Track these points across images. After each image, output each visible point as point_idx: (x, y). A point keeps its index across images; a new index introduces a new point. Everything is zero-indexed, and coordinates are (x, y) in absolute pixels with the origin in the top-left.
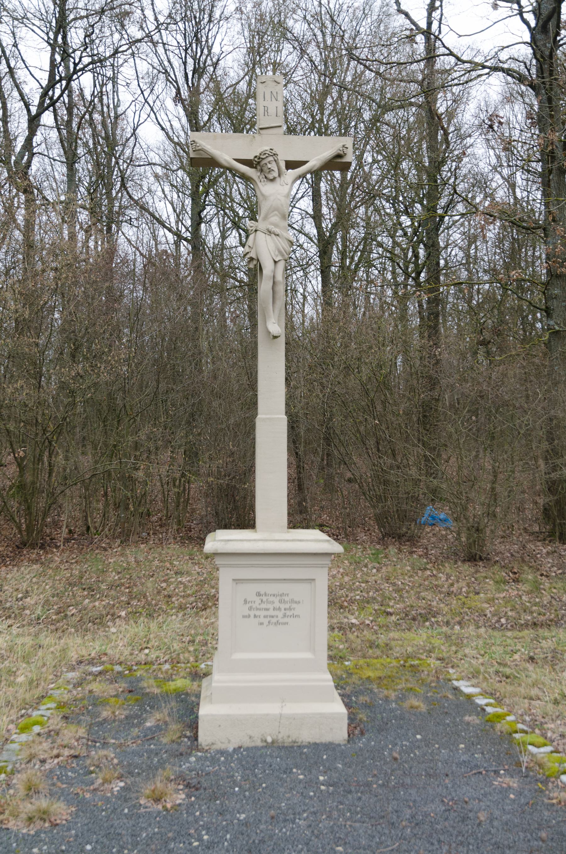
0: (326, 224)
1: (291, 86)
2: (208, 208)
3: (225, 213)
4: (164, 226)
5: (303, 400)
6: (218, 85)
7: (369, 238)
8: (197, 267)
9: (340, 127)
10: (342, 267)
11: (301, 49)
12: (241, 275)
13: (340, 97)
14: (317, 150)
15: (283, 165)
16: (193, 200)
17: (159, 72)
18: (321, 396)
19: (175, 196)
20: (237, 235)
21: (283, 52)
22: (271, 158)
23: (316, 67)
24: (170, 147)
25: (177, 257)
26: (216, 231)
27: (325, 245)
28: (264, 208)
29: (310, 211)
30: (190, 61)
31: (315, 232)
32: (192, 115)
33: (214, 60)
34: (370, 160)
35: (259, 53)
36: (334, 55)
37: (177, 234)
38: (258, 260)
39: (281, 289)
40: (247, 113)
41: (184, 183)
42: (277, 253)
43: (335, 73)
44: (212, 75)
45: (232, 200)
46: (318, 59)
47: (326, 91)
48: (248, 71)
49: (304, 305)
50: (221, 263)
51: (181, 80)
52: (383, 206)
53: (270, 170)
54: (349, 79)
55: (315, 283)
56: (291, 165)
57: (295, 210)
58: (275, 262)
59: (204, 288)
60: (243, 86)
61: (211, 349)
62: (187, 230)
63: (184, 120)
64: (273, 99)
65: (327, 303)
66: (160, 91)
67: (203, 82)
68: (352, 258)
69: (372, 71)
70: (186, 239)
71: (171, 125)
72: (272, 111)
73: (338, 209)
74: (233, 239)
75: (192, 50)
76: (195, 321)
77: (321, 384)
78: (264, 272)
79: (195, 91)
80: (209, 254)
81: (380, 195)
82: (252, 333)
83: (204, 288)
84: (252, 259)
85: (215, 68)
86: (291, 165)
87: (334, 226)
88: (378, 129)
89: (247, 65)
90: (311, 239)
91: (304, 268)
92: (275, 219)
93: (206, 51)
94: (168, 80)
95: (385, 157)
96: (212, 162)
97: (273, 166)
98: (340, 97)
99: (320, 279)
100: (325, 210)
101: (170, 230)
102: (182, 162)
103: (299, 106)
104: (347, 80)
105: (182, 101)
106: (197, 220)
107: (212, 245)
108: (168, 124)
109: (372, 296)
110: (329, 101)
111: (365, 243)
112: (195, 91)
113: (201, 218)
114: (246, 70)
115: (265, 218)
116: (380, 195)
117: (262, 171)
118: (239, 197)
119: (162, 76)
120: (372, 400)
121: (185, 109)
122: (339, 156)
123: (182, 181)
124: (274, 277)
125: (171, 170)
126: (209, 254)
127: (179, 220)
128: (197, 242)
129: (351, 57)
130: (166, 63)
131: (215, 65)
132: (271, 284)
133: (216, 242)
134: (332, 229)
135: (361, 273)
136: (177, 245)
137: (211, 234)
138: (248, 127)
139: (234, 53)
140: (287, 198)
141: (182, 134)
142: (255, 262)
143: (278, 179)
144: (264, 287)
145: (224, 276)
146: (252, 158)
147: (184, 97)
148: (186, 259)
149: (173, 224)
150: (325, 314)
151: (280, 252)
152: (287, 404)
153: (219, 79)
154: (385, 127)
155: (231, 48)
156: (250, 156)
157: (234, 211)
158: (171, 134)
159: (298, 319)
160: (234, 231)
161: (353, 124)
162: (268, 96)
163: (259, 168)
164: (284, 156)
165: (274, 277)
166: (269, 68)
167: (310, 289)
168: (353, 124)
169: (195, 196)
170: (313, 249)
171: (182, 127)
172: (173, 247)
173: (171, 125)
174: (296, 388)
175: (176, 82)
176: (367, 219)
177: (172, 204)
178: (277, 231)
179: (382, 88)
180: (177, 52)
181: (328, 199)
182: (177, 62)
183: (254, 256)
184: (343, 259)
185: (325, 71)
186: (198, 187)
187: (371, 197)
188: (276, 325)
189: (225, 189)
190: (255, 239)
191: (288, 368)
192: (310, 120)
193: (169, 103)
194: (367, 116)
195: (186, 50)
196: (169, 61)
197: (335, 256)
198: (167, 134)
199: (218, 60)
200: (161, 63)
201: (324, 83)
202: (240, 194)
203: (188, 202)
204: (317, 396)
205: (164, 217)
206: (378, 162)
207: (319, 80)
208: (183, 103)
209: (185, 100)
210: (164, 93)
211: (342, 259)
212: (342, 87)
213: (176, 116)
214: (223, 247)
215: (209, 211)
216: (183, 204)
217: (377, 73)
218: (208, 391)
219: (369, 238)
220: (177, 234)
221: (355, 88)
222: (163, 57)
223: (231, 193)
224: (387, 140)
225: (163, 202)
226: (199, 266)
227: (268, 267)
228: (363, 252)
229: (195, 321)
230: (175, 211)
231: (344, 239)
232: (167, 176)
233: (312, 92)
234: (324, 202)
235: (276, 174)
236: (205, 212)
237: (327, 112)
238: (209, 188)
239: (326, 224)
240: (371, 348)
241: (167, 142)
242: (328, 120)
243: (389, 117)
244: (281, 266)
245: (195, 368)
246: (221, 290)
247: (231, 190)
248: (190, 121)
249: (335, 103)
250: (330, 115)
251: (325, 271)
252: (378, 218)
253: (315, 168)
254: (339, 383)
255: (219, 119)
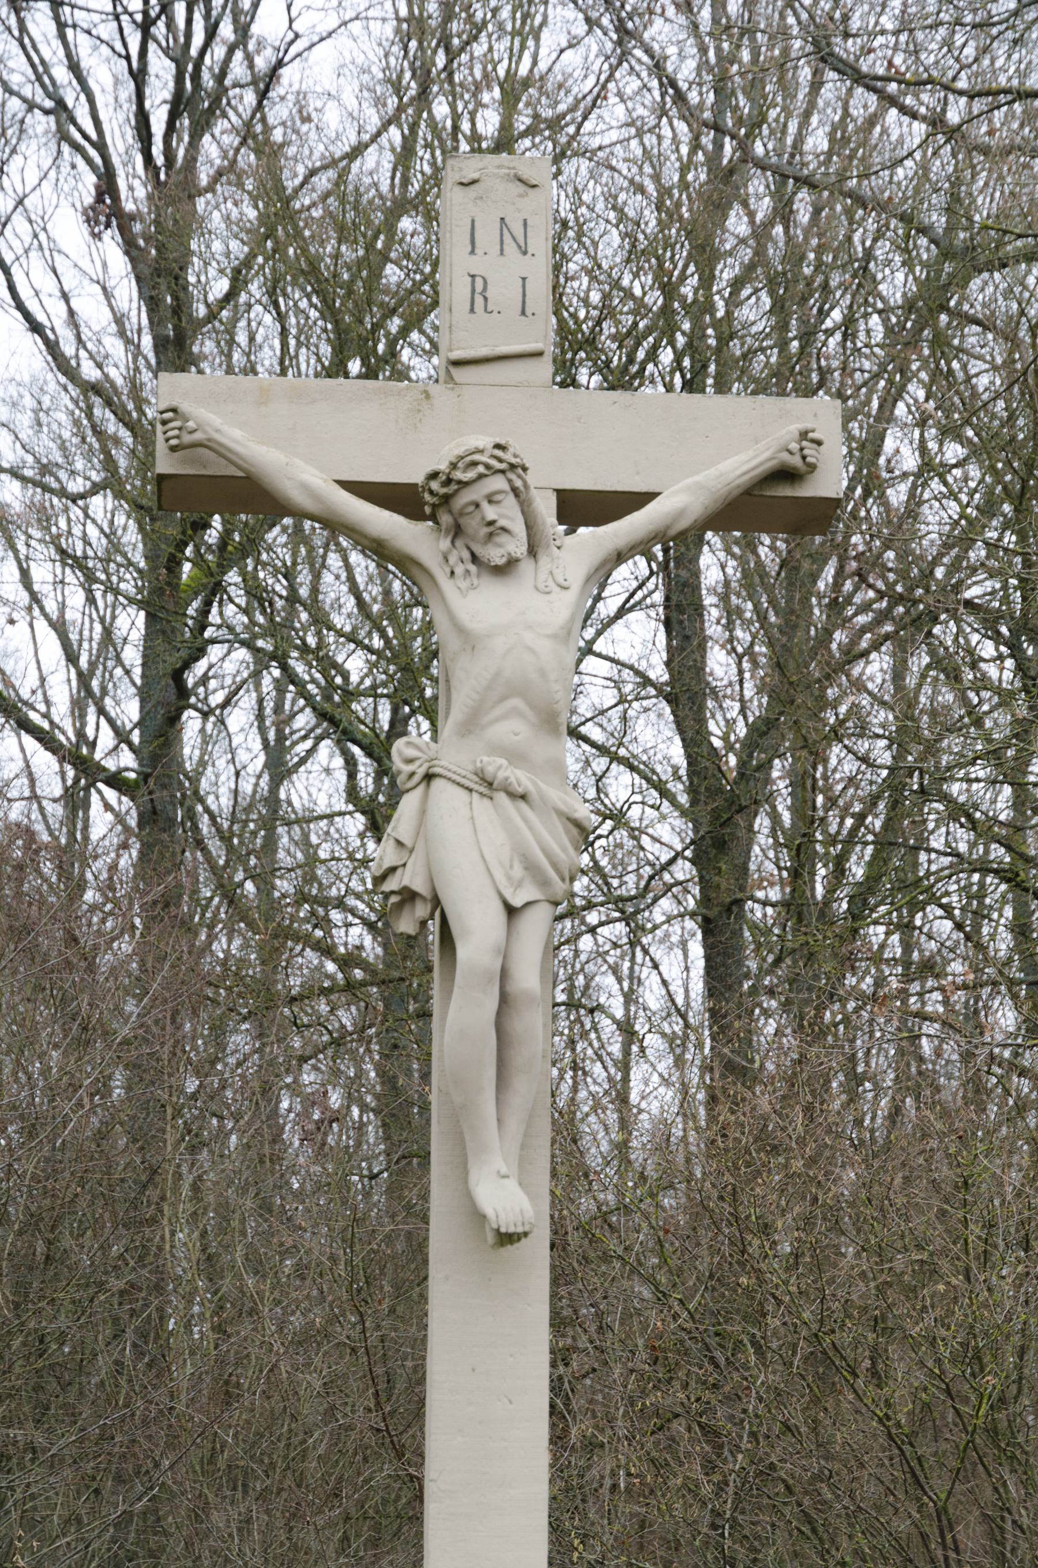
0: (726, 724)
1: (577, 168)
2: (215, 652)
3: (290, 676)
4: (25, 725)
5: (626, 1508)
6: (270, 153)
7: (910, 790)
8: (165, 908)
9: (783, 327)
10: (795, 906)
11: (621, 28)
12: (354, 936)
13: (784, 212)
14: (692, 448)
15: (546, 507)
16: (151, 618)
17: (31, 106)
18: (707, 1490)
19: (76, 598)
20: (338, 762)
21: (545, 35)
22: (498, 483)
23: (680, 97)
24: (63, 404)
25: (73, 854)
26: (253, 756)
27: (719, 808)
28: (465, 681)
29: (659, 673)
30: (161, 70)
31: (677, 752)
32: (161, 271)
33: (261, 63)
34: (910, 461)
35: (445, 42)
36: (755, 53)
37: (79, 759)
38: (436, 902)
39: (533, 1026)
40: (390, 269)
41: (115, 546)
42: (518, 871)
43: (758, 121)
44: (248, 125)
45: (321, 621)
46: (691, 64)
47: (725, 186)
48: (400, 109)
49: (625, 1067)
50: (264, 879)
51: (120, 139)
52: (970, 651)
53: (494, 530)
54: (818, 141)
55: (679, 965)
56: (580, 508)
57: (591, 664)
58: (511, 911)
59: (183, 990)
60: (377, 167)
61: (210, 1264)
62: (122, 736)
63: (127, 294)
64: (510, 247)
65: (733, 1067)
66: (32, 179)
67: (209, 148)
68: (839, 870)
69: (914, 116)
70: (115, 781)
71: (71, 313)
72: (503, 292)
73: (779, 666)
74: (319, 782)
75: (170, 25)
76: (143, 1139)
77: (710, 1433)
78: (462, 952)
79: (176, 187)
80: (215, 846)
81: (951, 602)
82: (393, 1190)
83: (183, 990)
84: (409, 896)
85: (262, 95)
86: (580, 508)
87: (762, 731)
88: (940, 342)
89: (398, 88)
90: (665, 793)
91: (630, 910)
92: (512, 728)
93: (226, 30)
94: (63, 136)
95: (975, 452)
96: (253, 498)
97: (507, 513)
98: (784, 212)
99: (697, 949)
100: (719, 664)
101: (46, 740)
102: (109, 464)
103: (611, 246)
104: (809, 144)
105: (123, 221)
106: (169, 696)
107: (226, 801)
108: (58, 310)
109: (931, 1028)
110: (737, 223)
111: (894, 805)
112: (176, 187)
113: (183, 692)
114: (392, 102)
115: (470, 726)
116: (951, 602)
117: (457, 531)
118: (350, 603)
119: (41, 124)
120: (941, 1512)
121: (130, 247)
122: (785, 475)
123: (110, 535)
124: (504, 974)
125: (62, 493)
126: (215, 846)
127: (87, 696)
128: (160, 788)
129: (824, 56)
130: (61, 73)
131: (265, 84)
132: (492, 1004)
133: (247, 787)
134: (751, 744)
135: (877, 933)
136: (75, 801)
137: (226, 757)
138: (395, 324)
139: (341, 40)
140: (563, 644)
141: (115, 347)
142: (421, 910)
143: (526, 566)
144: (461, 1019)
145: (278, 939)
146: (417, 478)
147: (129, 206)
148: (113, 868)
149: (61, 710)
150: (724, 1115)
151: (531, 868)
152: (555, 1528)
153: (277, 135)
154: (972, 336)
155: (333, 22)
156: (410, 471)
157: (328, 665)
158: (68, 348)
159: (598, 1138)
160: (326, 747)
161: (837, 315)
162: (488, 235)
163: (445, 519)
164: (551, 472)
165: (504, 974)
166: (486, 97)
167: (652, 996)
168: (837, 315)
169: (161, 603)
170: (669, 833)
171: (119, 320)
172: (56, 811)
173: (71, 313)
174: (592, 1446)
175: (101, 146)
176: (903, 701)
177: (59, 627)
178: (521, 778)
179: (956, 181)
180: (107, 30)
181: (731, 615)
182: (105, 73)
183: (419, 885)
184: (798, 875)
185: (718, 109)
186: (174, 564)
187: (912, 617)
188: (512, 1184)
189: (289, 575)
190: (423, 811)
191: (559, 1356)
192: (655, 299)
193: (69, 229)
194: (895, 284)
195: (146, 27)
196: (74, 67)
197: (764, 855)
198: (52, 347)
199: (280, 64)
200: (41, 72)
201: (713, 159)
202: (355, 590)
203: (131, 624)
204: (691, 1488)
205: (26, 686)
206: (942, 471)
207: (696, 146)
208: (122, 229)
209: (132, 217)
210: (47, 186)
211: (795, 874)
212: (788, 177)
213: (94, 283)
214: (271, 811)
215: (224, 663)
216: (108, 632)
217: (936, 122)
218: (194, 1457)
219: (910, 790)
220: (79, 759)
221: (844, 183)
222: (52, 51)
223: (315, 590)
224: (983, 381)
225: (22, 626)
226: (169, 901)
227: (478, 932)
228: (884, 844)
229: (143, 1139)
230: (72, 658)
231: (803, 785)
232: (45, 518)
233: (664, 192)
234: (713, 630)
235: (517, 546)
236: (200, 667)
237: (726, 273)
238: (224, 569)
239: (726, 724)
240: (929, 1271)
241: (53, 380)
242: (733, 302)
243: (983, 291)
244: (536, 925)
245: (139, 1352)
246: (264, 1002)
247: (317, 577)
248: (152, 303)
249: (761, 234)
250: (737, 284)
251: (719, 921)
252: (948, 697)
253: (683, 524)
254: (787, 1428)
255: (273, 292)
